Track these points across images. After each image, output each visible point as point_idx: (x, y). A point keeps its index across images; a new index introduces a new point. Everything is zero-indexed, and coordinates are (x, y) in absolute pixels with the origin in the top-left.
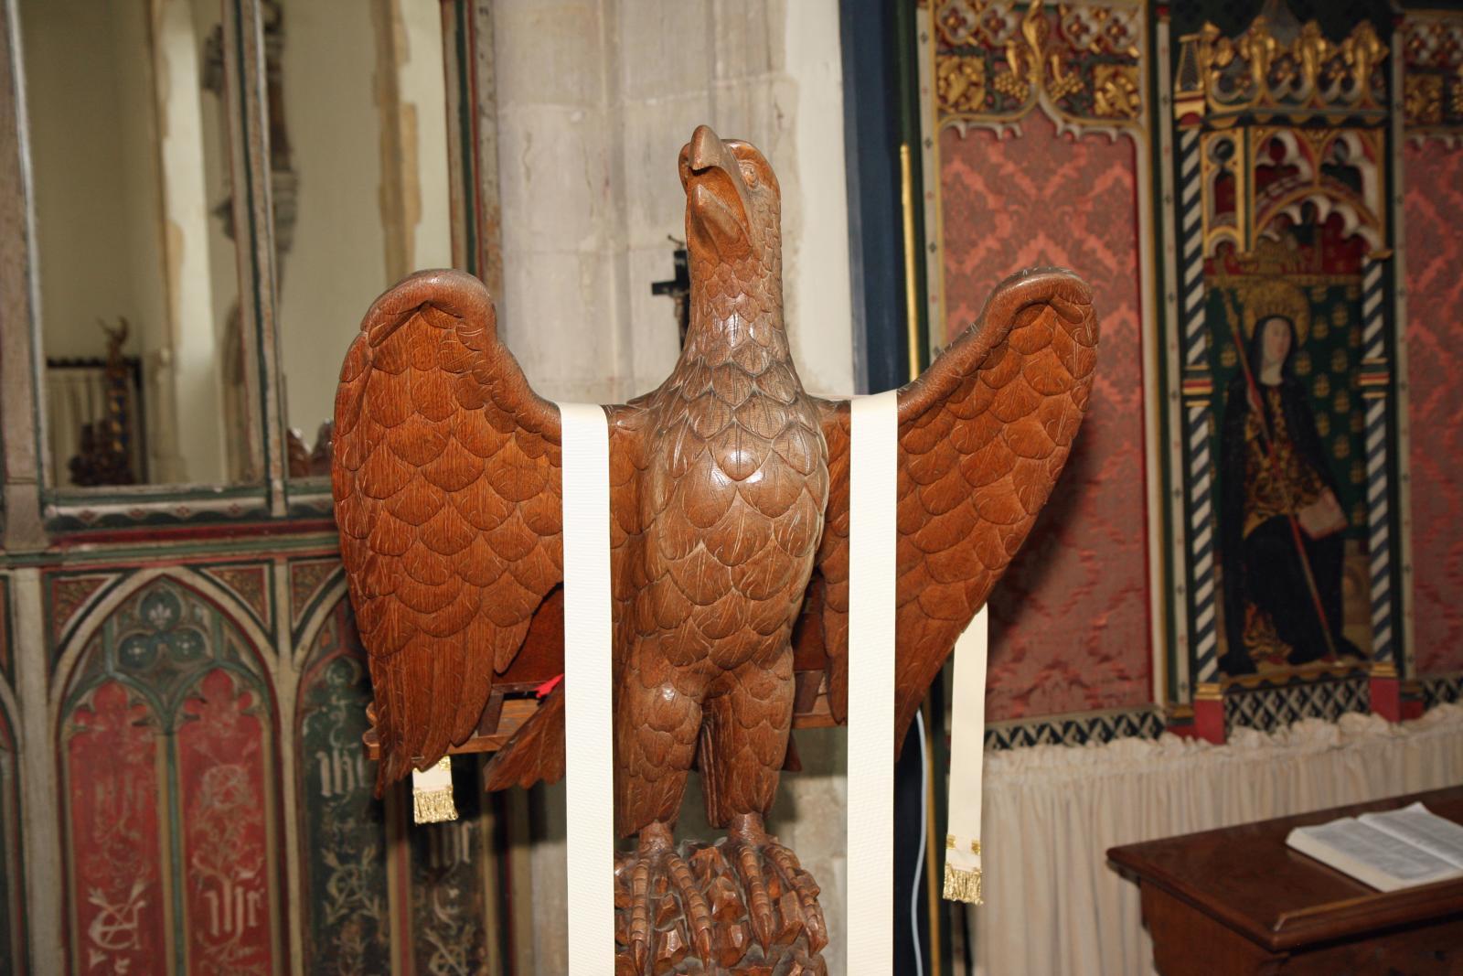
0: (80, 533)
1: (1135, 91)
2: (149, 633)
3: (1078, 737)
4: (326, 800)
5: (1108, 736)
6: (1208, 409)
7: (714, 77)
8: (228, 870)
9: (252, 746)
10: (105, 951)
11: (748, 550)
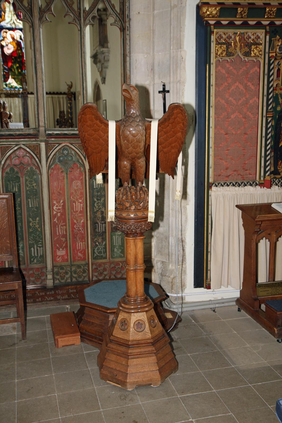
0: (52, 136)
1: (261, 51)
2: (64, 156)
3: (238, 185)
4: (95, 189)
5: (245, 185)
6: (272, 119)
7: (171, 50)
8: (77, 200)
9: (81, 177)
10: (56, 211)
11: (132, 142)
